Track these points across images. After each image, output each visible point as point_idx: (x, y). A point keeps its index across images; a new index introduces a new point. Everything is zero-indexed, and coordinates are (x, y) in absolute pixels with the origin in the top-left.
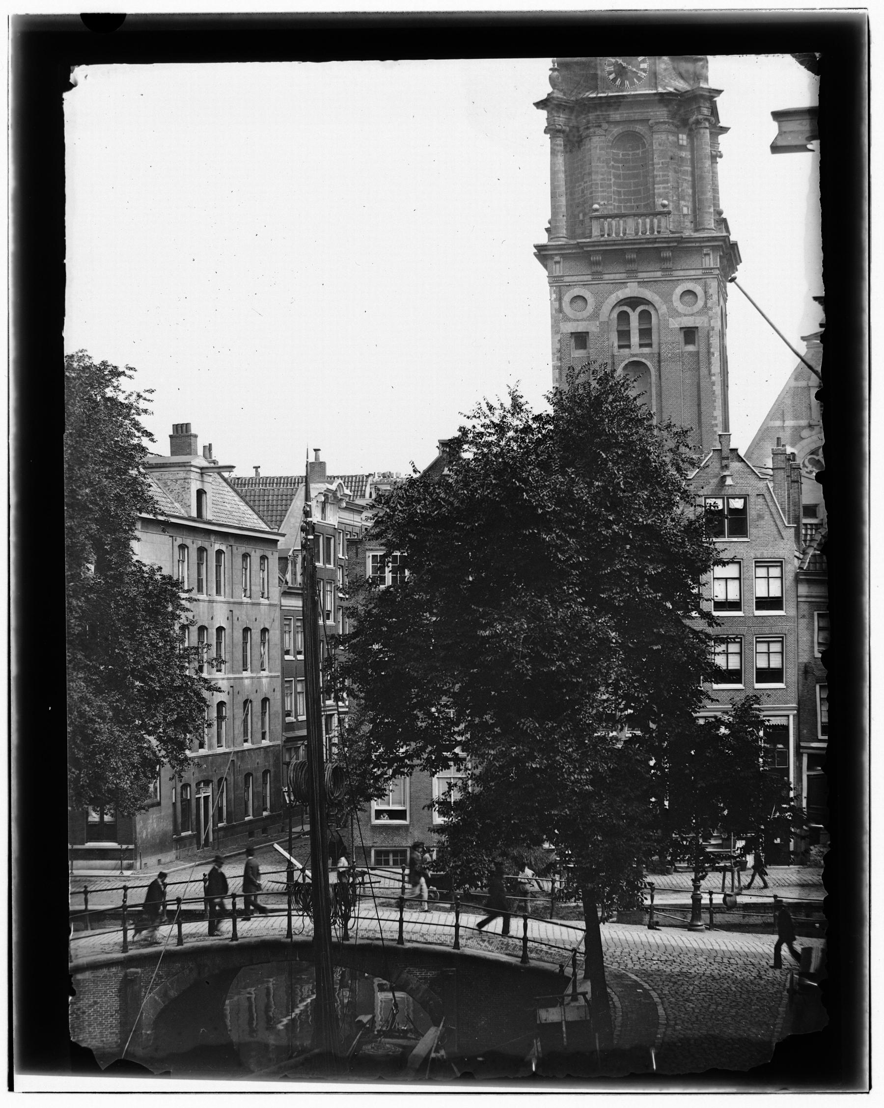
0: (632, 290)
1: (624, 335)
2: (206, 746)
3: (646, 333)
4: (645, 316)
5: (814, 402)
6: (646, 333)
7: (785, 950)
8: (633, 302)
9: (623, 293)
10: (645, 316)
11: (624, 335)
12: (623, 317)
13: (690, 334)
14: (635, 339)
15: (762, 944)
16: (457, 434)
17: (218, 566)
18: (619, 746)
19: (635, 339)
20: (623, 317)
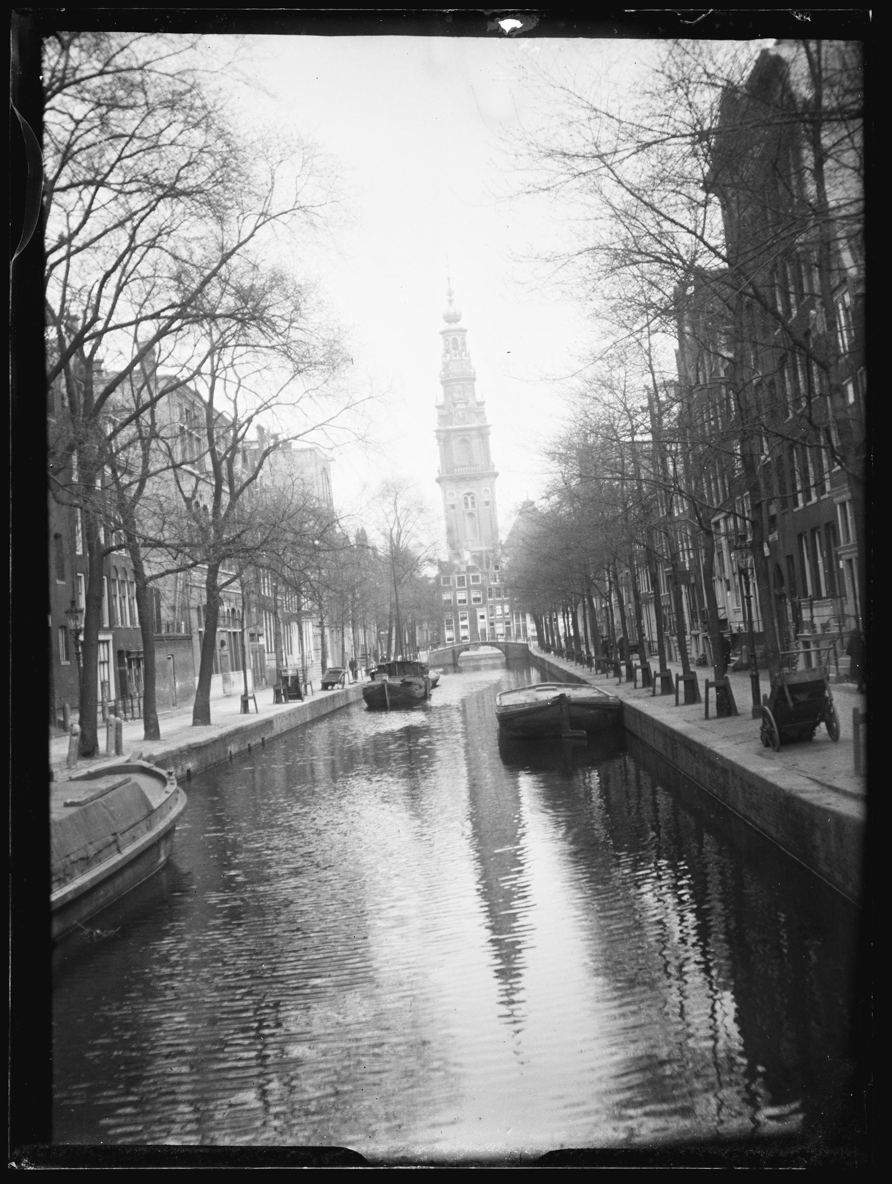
0: (468, 490)
1: (466, 504)
2: (494, 595)
3: (473, 503)
4: (473, 498)
5: (401, 1154)
6: (473, 503)
7: (62, 182)
8: (469, 494)
9: (466, 491)
10: (473, 498)
11: (466, 504)
12: (466, 499)
13: (487, 503)
14: (470, 505)
15: (672, 474)
16: (759, 722)
17: (301, 639)
18: (431, 582)
19: (470, 505)
20: (466, 499)
